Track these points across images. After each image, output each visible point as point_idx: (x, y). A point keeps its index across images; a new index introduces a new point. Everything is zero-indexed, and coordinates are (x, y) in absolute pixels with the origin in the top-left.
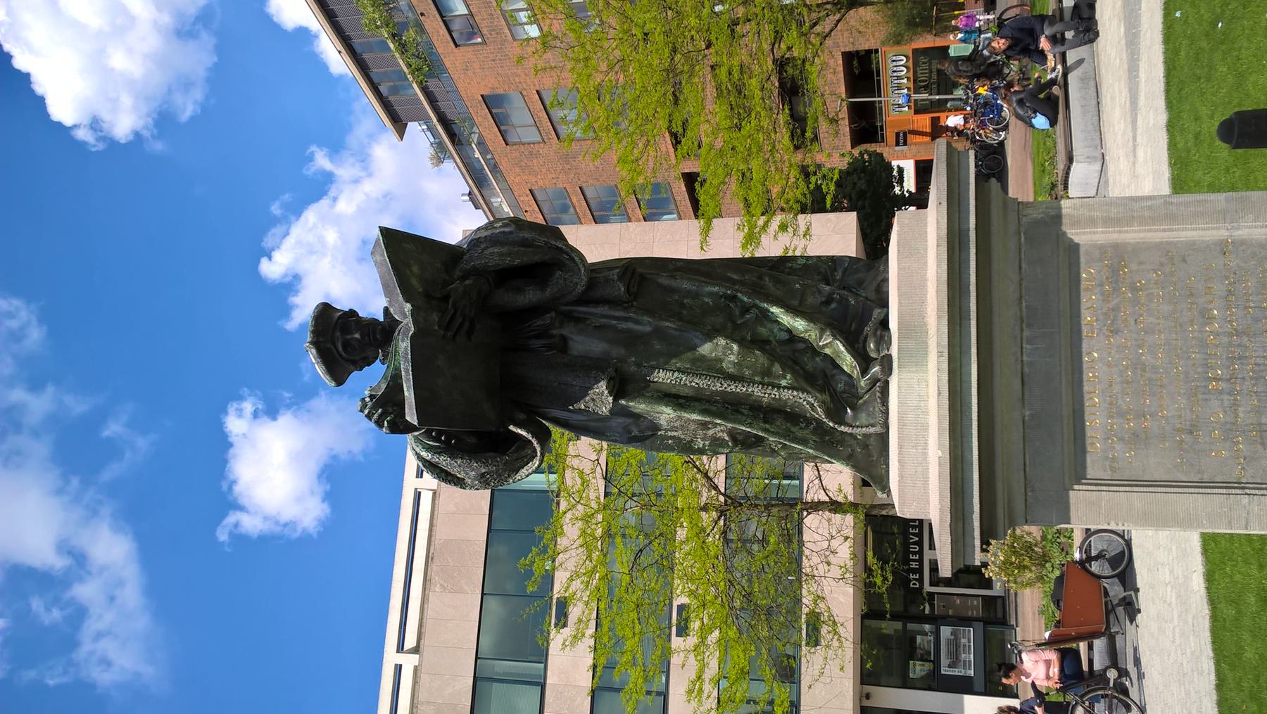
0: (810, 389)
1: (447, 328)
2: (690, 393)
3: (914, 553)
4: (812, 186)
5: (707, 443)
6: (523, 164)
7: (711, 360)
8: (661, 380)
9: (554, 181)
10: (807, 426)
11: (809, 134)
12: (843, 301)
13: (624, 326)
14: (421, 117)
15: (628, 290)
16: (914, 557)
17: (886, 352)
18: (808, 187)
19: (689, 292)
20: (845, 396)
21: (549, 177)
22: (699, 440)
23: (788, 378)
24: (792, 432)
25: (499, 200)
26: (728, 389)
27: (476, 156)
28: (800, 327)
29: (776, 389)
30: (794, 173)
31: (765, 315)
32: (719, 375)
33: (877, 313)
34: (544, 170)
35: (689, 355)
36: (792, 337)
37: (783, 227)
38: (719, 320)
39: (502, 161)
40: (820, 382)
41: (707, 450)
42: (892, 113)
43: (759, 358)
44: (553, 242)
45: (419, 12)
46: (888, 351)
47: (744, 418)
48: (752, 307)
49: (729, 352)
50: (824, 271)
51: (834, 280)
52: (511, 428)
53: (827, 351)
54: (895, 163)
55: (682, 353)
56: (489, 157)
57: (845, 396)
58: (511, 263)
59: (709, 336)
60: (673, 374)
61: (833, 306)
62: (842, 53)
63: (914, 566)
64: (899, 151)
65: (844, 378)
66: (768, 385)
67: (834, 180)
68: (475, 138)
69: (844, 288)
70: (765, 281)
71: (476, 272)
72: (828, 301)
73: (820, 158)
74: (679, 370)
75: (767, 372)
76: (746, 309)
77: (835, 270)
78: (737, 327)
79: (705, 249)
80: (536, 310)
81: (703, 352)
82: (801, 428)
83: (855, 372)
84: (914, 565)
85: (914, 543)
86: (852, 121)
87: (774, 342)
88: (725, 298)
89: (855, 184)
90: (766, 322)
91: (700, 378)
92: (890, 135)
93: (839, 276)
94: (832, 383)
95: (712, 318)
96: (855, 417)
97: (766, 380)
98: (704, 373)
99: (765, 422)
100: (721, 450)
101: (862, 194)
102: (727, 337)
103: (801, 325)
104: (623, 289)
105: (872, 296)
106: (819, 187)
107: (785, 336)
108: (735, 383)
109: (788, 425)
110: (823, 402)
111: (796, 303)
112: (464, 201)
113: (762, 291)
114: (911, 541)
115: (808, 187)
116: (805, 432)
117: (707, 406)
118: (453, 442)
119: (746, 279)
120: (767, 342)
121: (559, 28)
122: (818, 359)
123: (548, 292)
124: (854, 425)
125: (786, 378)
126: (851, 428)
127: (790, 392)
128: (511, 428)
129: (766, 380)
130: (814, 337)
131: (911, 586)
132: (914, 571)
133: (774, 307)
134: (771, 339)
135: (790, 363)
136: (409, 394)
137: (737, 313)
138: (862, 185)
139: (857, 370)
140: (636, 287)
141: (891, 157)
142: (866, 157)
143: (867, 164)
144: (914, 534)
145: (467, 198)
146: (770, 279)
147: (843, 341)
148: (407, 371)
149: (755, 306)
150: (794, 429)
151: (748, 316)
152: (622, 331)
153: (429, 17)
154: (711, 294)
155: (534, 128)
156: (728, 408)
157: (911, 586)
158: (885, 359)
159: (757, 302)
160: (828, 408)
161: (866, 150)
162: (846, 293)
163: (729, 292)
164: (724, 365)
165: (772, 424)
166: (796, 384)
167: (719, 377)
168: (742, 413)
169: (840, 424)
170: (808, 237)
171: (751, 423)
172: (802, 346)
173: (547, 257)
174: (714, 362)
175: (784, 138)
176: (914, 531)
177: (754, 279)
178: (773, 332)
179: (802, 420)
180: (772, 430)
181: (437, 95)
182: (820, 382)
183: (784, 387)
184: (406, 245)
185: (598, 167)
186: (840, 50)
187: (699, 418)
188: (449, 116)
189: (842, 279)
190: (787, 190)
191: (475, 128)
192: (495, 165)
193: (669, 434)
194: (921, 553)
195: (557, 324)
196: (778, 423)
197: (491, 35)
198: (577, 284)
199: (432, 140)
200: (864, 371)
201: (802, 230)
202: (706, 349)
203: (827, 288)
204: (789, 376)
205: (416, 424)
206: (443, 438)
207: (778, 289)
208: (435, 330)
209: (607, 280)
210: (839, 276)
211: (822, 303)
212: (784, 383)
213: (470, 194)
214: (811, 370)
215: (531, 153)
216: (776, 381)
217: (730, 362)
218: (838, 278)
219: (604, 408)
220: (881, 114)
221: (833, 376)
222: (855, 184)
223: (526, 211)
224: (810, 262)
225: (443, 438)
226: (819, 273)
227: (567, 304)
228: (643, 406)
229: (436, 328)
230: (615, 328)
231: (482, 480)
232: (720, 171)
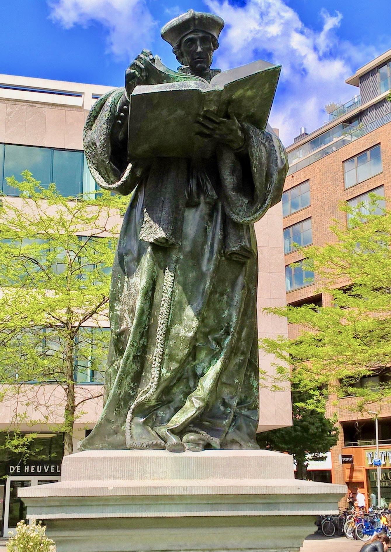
0: (159, 390)
1: (205, 117)
2: (156, 300)
3: (35, 469)
4: (311, 392)
5: (118, 313)
6: (328, 175)
7: (181, 316)
8: (166, 278)
9: (316, 198)
10: (131, 388)
11: (351, 390)
12: (225, 415)
14: (363, 98)
15: (233, 253)
16: (32, 469)
17: (187, 448)
18: (311, 389)
19: (232, 299)
20: (154, 417)
21: (319, 194)
22: (121, 307)
23: (168, 374)
24: (126, 377)
25: (301, 156)
26: (159, 329)
27: (334, 139)
29: (159, 365)
30: (322, 379)
31: (215, 356)
32: (169, 322)
33: (215, 441)
34: (323, 190)
35: (185, 300)
36: (197, 377)
37: (281, 370)
38: (211, 322)
39: (331, 159)
40: (164, 398)
41: (113, 313)
42: (367, 452)
43: (182, 352)
44: (269, 197)
46: (188, 449)
47: (137, 341)
48: (221, 346)
49: (187, 330)
50: (248, 401)
51: (241, 409)
52: (130, 166)
53: (188, 403)
54: (328, 454)
55: (186, 294)
56: (334, 149)
57: (154, 417)
58: (254, 165)
59: (199, 315)
60: (170, 287)
61: (222, 408)
63: (26, 469)
64: (338, 457)
65: (167, 416)
66: (162, 359)
67: (316, 409)
68: (348, 138)
69: (235, 416)
70: (240, 356)
71: (247, 139)
72: (224, 404)
73: (333, 398)
74: (173, 292)
75: (171, 358)
76: (219, 342)
77: (249, 409)
78: (206, 335)
79: (265, 311)
80: (218, 184)
81: (186, 310)
82: (129, 384)
83: (172, 425)
84: (27, 469)
85: (43, 469)
86: (361, 422)
87: (194, 363)
88: (228, 327)
89: (313, 424)
90: (209, 357)
92: (349, 451)
93: (244, 412)
94: (164, 407)
95: (212, 317)
96: (138, 424)
97: (166, 358)
98: (171, 311)
99: (134, 357)
100: (113, 323)
101: (305, 429)
102: (198, 328)
105: (229, 437)
106: (311, 397)
107: (199, 371)
108: (164, 334)
109: (132, 374)
110: (149, 401)
111: (224, 380)
112: (301, 130)
113: (233, 354)
114: (45, 467)
115: (311, 389)
116: (127, 387)
117: (146, 313)
118: (119, 121)
119: (242, 342)
120: (195, 358)
122: (181, 396)
124: (132, 423)
128: (130, 166)
129: (166, 358)
130: (198, 393)
131: (11, 467)
132: (22, 469)
133: (221, 364)
134: (197, 361)
135: (179, 375)
137: (216, 336)
138: (313, 430)
139: (173, 426)
140: (235, 259)
141: (334, 452)
142: (334, 433)
143: (328, 433)
144: (50, 469)
145: (303, 132)
146: (242, 360)
147: (195, 415)
149: (222, 349)
150: (129, 379)
151: (214, 344)
152: (203, 249)
154: (230, 316)
155: (355, 183)
156: (145, 328)
157: (11, 467)
158: (181, 447)
159: (225, 351)
160: (145, 404)
161: (338, 433)
162: (231, 417)
164: (177, 326)
165: (133, 361)
166: (162, 380)
167: (168, 322)
168: (141, 339)
170: (274, 389)
172: (192, 384)
173: (258, 192)
174: (179, 319)
175: (347, 371)
176: (52, 469)
177: (242, 348)
178: (201, 362)
179: (136, 384)
180: (128, 362)
181: (380, 109)
182: (164, 398)
183: (160, 371)
184: (267, 86)
185: (326, 231)
188: (364, 119)
189: (241, 414)
190: (309, 373)
191: (355, 138)
192: (328, 153)
193: (125, 284)
194: (36, 474)
195: (208, 200)
196: (133, 366)
198: (238, 215)
199: (347, 106)
200: (172, 431)
201: (279, 384)
202: (189, 312)
203: (235, 404)
204: (169, 374)
207: (234, 366)
208: (203, 108)
209: (241, 238)
210: (244, 412)
211: (224, 399)
212: (164, 371)
213: (306, 134)
214: (173, 391)
215: (336, 180)
216: (165, 365)
217: (179, 330)
218: (243, 411)
219: (145, 235)
220: (366, 444)
221: (169, 408)
222: (313, 424)
223: (293, 176)
224: (255, 391)
225: (122, 114)
226: (246, 398)
227: (223, 207)
228: (146, 264)
229: (205, 109)
231: (90, 143)
232: (323, 323)
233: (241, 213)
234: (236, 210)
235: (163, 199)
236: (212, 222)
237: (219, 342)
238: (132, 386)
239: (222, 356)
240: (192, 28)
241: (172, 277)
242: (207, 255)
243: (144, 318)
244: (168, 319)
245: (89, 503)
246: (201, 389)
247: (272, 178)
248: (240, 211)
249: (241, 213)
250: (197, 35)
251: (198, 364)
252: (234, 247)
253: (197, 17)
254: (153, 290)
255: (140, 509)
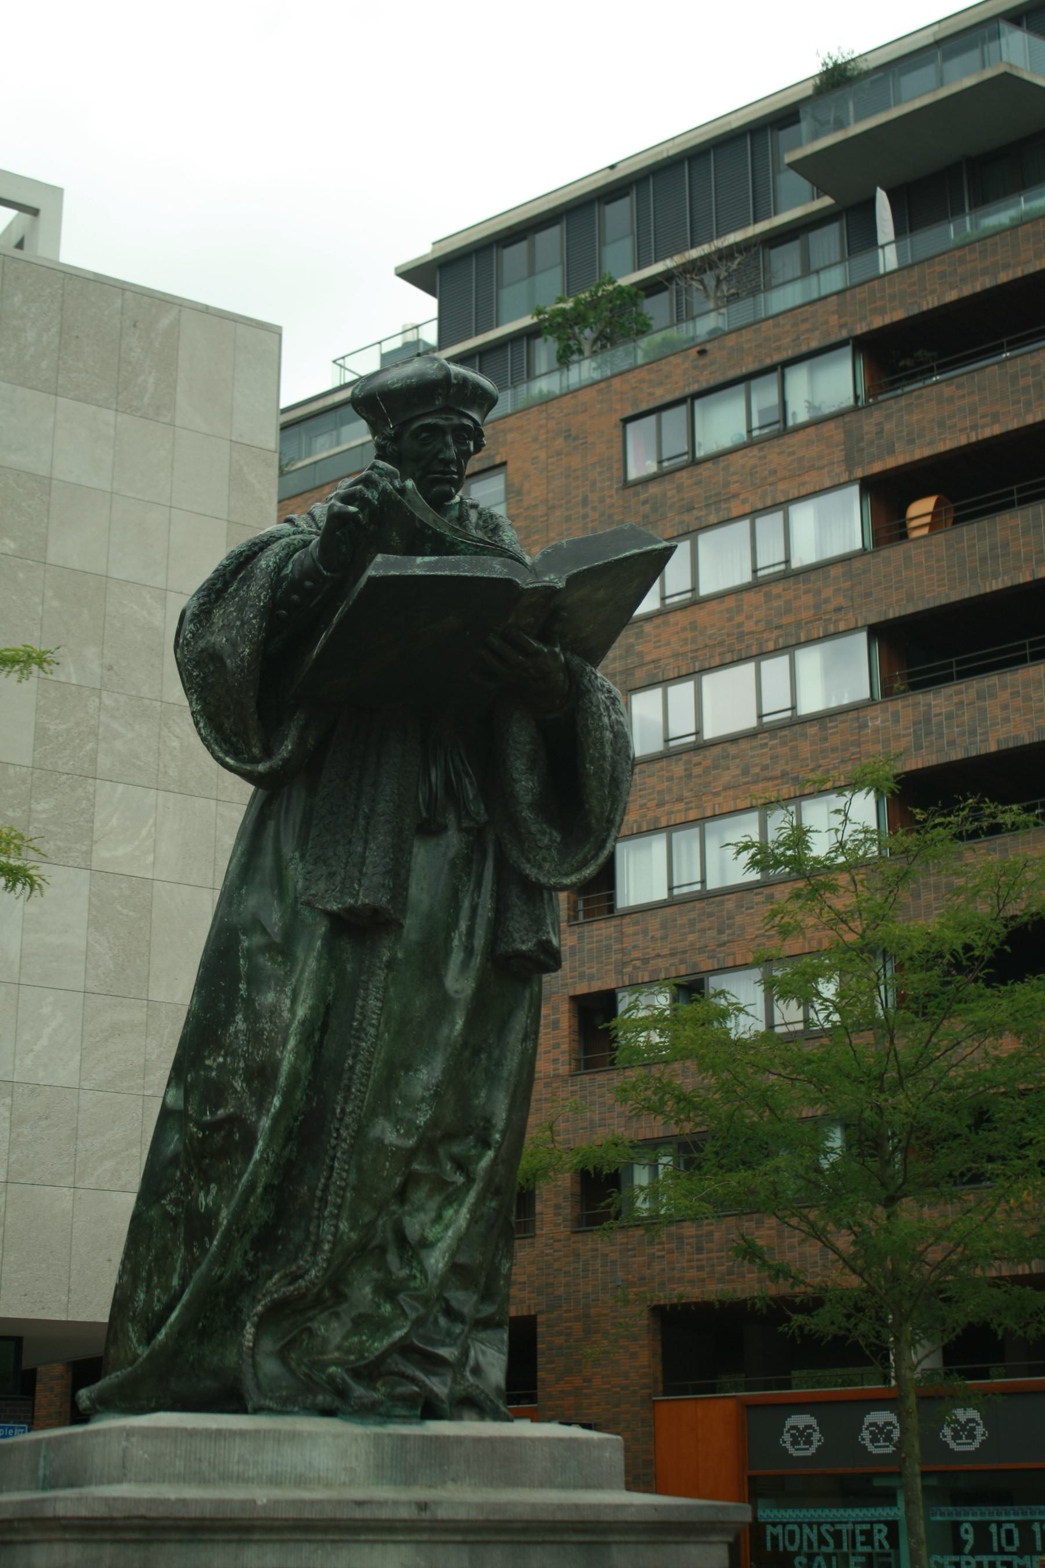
10: (247, 1264)
13: (456, 942)
19: (499, 1064)
23: (352, 1234)
24: (242, 1236)
28: (432, 1261)
45: (708, 347)
49: (402, 1131)
62: (534, 1317)
82: (246, 1253)
88: (485, 1128)
91: (364, 1075)
98: (370, 1083)
99: (268, 1188)
100: (195, 1099)
103: (437, 1262)
104: (524, 948)
116: (239, 1260)
121: (647, 659)
123: (526, 813)
125: (352, 1229)
126: (251, 1344)
127: (330, 1237)
134: (406, 1208)
136: (421, 565)
146: (494, 1209)
148: (455, 566)
149: (470, 1180)
150: (247, 1238)
151: (448, 1168)
152: (449, 939)
153: (695, 367)
156: (296, 1120)
163: (497, 1136)
165: (262, 1199)
168: (284, 1146)
169: (258, 1327)
171: (267, 1161)
179: (260, 1254)
186: (542, 1312)
187: (285, 1067)
195: (466, 824)
196: (261, 1211)
197: (645, 502)
205: (371, 572)
206: (295, 597)
212: (344, 1226)
225: (295, 597)
228: (312, 964)
230: (454, 925)
233: (547, 866)
234: (535, 857)
235: (366, 810)
236: (469, 875)
237: (462, 1165)
238: (251, 1260)
239: (471, 1197)
240: (438, 402)
241: (377, 999)
242: (456, 958)
243: (299, 1095)
244: (362, 1101)
245: (206, 1537)
246: (418, 1275)
247: (618, 789)
248: (544, 859)
249: (547, 866)
250: (446, 419)
251: (410, 1214)
252: (523, 942)
253: (455, 381)
254: (324, 1028)
255: (320, 1552)
